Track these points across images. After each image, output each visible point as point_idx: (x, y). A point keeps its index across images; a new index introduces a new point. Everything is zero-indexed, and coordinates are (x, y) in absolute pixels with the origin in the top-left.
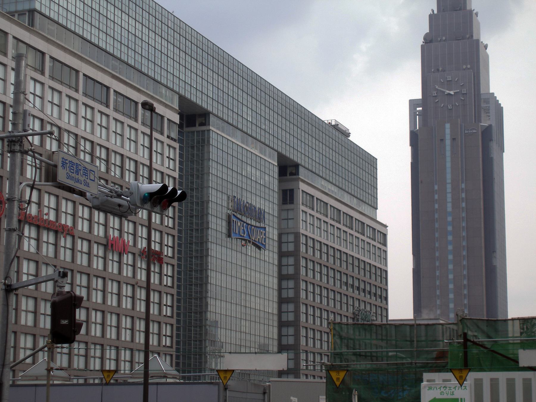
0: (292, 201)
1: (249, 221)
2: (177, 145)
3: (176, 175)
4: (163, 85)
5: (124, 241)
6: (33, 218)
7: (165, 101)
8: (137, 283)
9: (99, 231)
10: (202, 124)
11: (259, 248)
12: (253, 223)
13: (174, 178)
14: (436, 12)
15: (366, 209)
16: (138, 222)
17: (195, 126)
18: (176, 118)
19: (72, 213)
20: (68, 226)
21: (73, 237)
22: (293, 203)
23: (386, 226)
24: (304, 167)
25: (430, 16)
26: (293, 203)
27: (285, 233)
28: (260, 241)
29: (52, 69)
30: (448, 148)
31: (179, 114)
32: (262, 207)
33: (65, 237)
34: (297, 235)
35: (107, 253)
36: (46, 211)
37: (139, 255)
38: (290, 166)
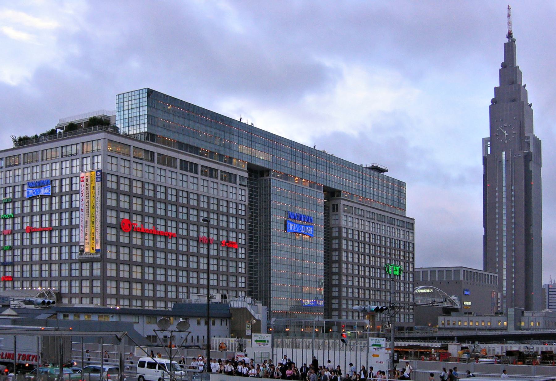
10: (268, 175)
13: (245, 205)
15: (398, 211)
18: (246, 175)
23: (414, 219)
29: (222, 176)
30: (504, 166)
34: (340, 229)
37: (121, 229)
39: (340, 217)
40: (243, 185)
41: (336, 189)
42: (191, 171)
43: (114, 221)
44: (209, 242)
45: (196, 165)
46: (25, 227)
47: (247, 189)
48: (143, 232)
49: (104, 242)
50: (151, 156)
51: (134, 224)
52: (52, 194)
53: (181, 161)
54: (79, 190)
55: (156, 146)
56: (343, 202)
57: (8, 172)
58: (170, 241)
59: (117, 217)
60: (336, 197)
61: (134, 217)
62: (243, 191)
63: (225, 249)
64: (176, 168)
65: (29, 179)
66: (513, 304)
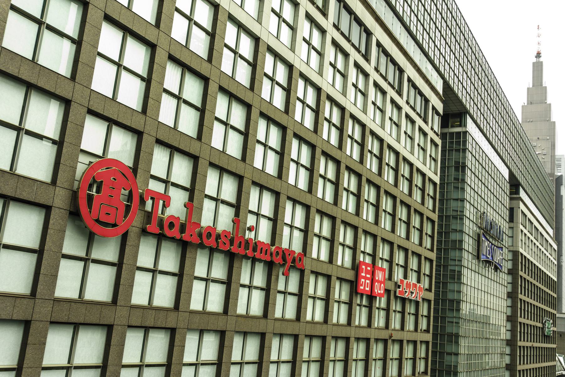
2: (438, 141)
6: (218, 236)
8: (391, 337)
14: (526, 104)
17: (448, 127)
19: (271, 216)
20: (294, 252)
21: (302, 272)
25: (523, 106)
33: (286, 274)
36: (251, 220)
48: (187, 239)
51: (155, 197)
59: (64, 144)
61: (159, 160)
66: (454, 320)
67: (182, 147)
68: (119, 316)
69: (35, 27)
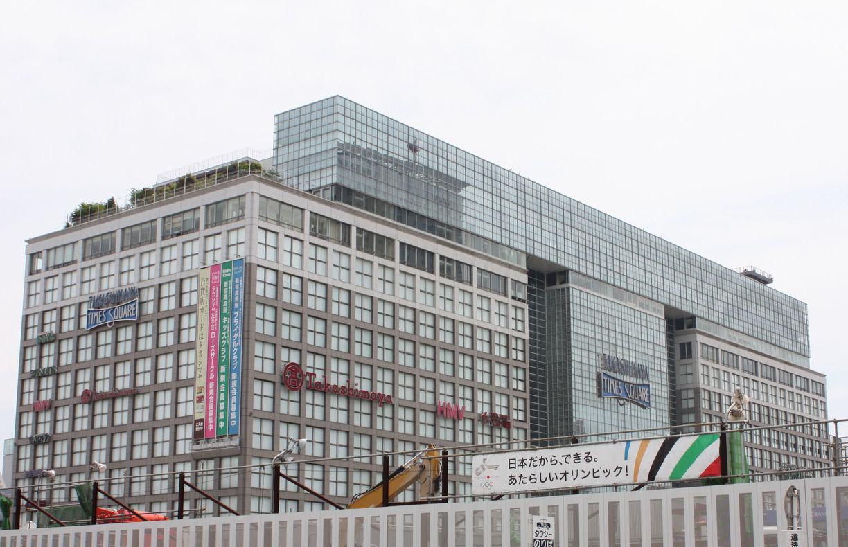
0: (690, 356)
1: (627, 379)
3: (526, 336)
4: (505, 245)
5: (458, 408)
7: (507, 262)
9: (426, 398)
10: (564, 282)
11: (644, 407)
12: (633, 380)
16: (476, 387)
18: (524, 278)
22: (691, 357)
23: (823, 376)
24: (701, 318)
26: (691, 357)
27: (684, 390)
28: (642, 399)
29: (479, 279)
31: (527, 274)
32: (645, 364)
34: (697, 391)
35: (437, 420)
37: (282, 384)
38: (687, 319)
39: (696, 370)
40: (519, 300)
41: (687, 313)
42: (421, 268)
43: (268, 367)
44: (457, 416)
45: (432, 255)
46: (80, 393)
47: (526, 306)
48: (324, 389)
49: (246, 413)
50: (344, 233)
51: (310, 374)
52: (140, 316)
53: (402, 244)
54: (194, 342)
55: (354, 212)
56: (700, 338)
57: (50, 280)
58: (379, 411)
60: (685, 329)
61: (309, 360)
62: (519, 312)
63: (487, 431)
64: (393, 259)
65: (92, 290)
67: (319, 316)
68: (302, 422)
69: (262, 321)
